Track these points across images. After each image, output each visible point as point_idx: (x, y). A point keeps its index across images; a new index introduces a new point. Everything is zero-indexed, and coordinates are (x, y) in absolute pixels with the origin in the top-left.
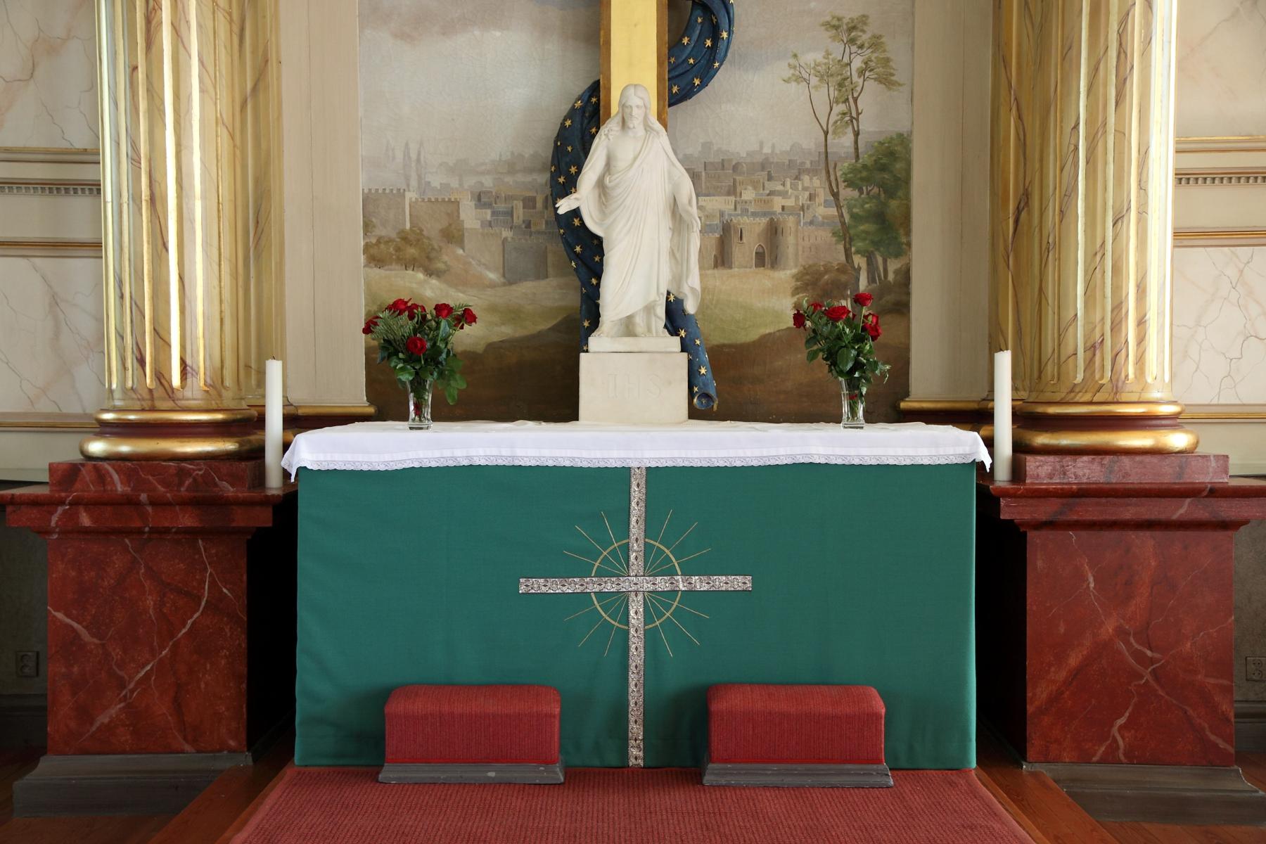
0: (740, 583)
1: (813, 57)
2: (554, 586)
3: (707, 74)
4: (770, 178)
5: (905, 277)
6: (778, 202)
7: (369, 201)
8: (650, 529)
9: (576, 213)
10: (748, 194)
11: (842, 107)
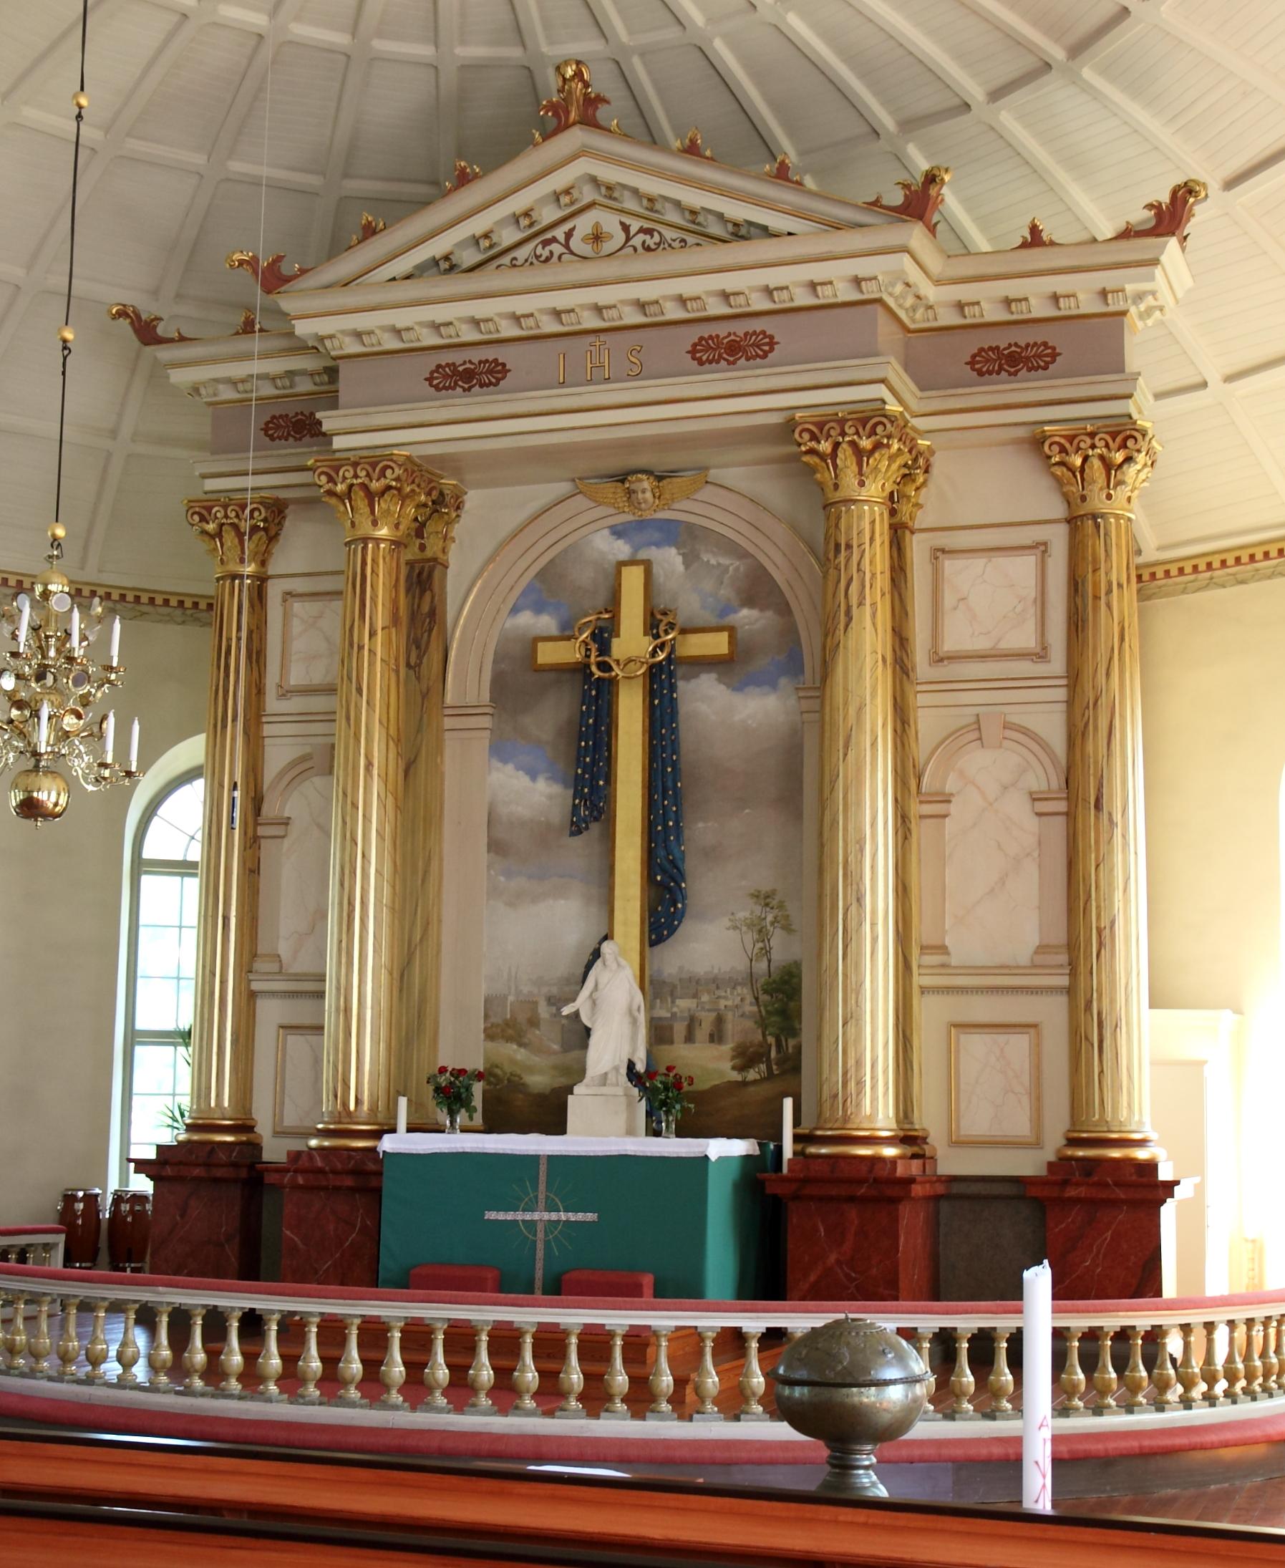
0: (591, 1217)
1: (742, 915)
2: (501, 1216)
3: (672, 930)
4: (718, 988)
5: (798, 1049)
6: (723, 1003)
7: (488, 1001)
8: (548, 1188)
9: (576, 1015)
10: (705, 998)
11: (761, 945)
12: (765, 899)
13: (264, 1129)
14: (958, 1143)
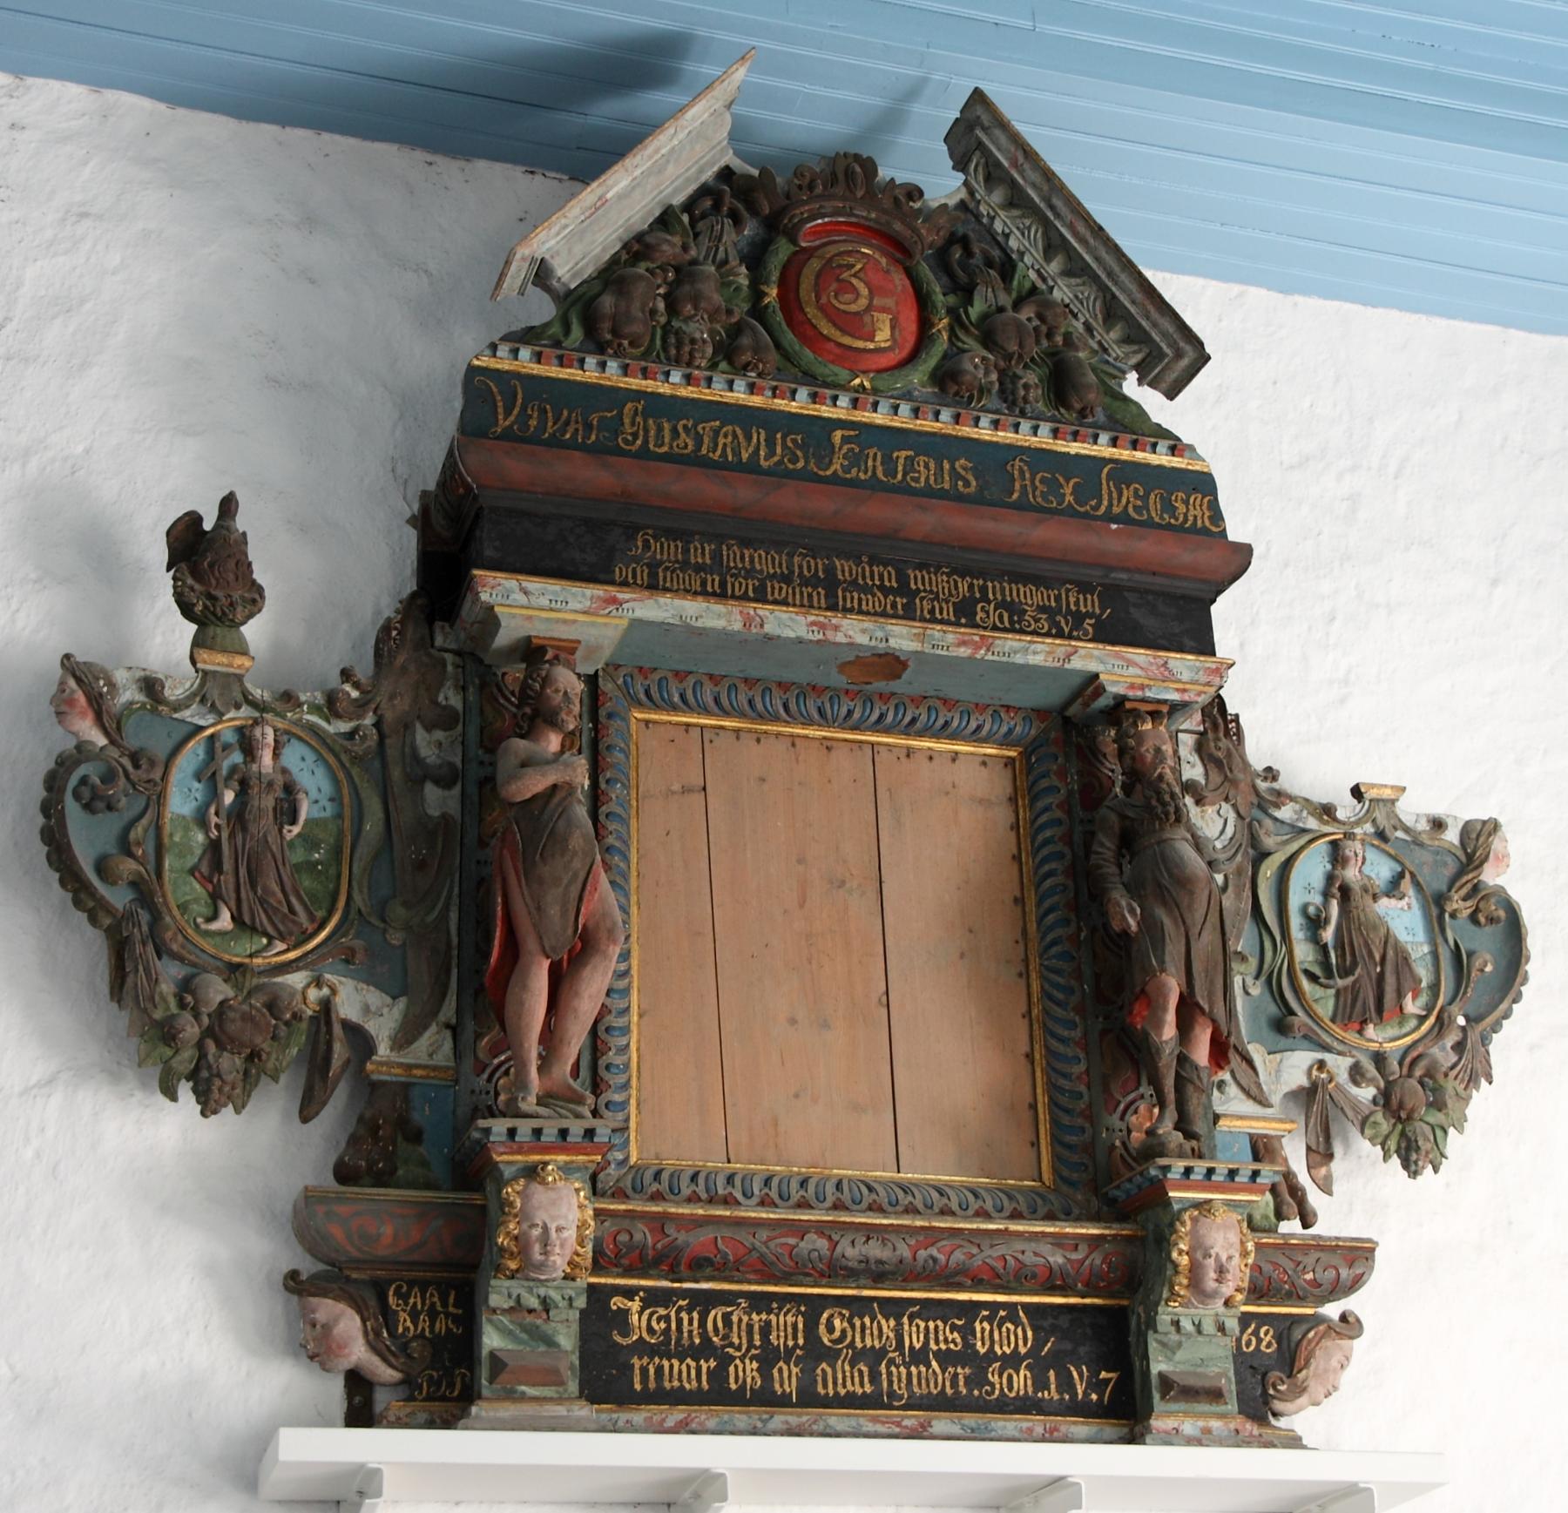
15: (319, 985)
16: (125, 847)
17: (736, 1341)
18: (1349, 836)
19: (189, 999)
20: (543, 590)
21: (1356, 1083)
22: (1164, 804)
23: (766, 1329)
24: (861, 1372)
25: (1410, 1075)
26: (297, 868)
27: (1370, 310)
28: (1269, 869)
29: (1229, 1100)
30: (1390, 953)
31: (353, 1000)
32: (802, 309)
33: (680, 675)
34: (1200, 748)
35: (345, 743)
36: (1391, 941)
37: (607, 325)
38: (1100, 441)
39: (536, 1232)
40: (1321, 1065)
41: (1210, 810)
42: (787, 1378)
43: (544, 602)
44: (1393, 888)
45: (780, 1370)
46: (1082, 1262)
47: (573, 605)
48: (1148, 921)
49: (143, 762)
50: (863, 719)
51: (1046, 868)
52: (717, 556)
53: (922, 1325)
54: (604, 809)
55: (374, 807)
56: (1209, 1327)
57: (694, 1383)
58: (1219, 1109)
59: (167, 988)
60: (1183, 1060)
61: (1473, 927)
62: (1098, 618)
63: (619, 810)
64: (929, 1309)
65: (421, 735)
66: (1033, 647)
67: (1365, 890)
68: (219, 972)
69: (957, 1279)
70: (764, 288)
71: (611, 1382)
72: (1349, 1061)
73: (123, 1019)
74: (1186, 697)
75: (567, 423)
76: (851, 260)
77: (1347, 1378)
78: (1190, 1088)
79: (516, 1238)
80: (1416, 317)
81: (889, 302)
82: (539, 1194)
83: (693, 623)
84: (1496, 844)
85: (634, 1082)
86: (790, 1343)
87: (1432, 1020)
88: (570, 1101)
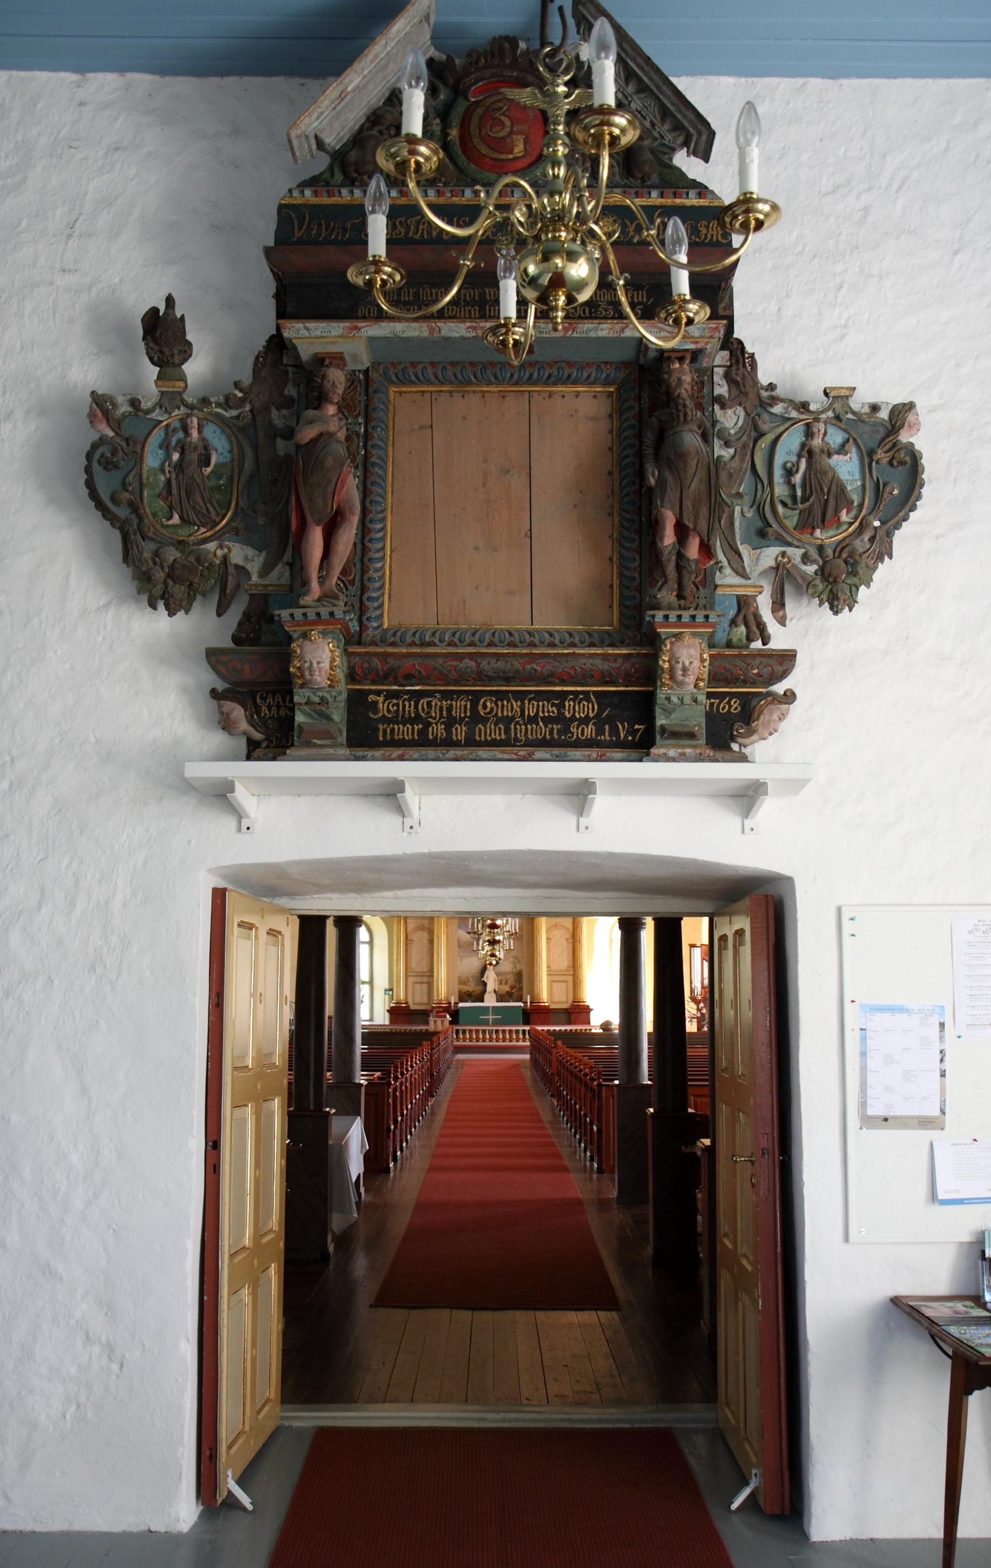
12: (515, 957)
13: (410, 1003)
14: (414, 1004)
15: (222, 548)
16: (124, 486)
17: (433, 715)
18: (817, 420)
19: (157, 560)
20: (318, 328)
21: (805, 563)
22: (678, 411)
23: (450, 709)
24: (500, 729)
25: (839, 557)
26: (212, 489)
27: (893, 81)
28: (764, 444)
29: (725, 576)
30: (834, 487)
31: (239, 554)
32: (471, 141)
33: (413, 365)
34: (727, 376)
35: (235, 421)
36: (835, 480)
37: (352, 168)
38: (690, 195)
39: (307, 665)
40: (783, 554)
41: (730, 412)
42: (460, 732)
43: (318, 333)
44: (842, 450)
45: (456, 729)
46: (619, 668)
47: (334, 333)
48: (661, 482)
49: (131, 443)
50: (520, 378)
51: (625, 453)
52: (416, 295)
53: (536, 704)
54: (370, 443)
55: (249, 453)
56: (688, 700)
57: (410, 737)
58: (718, 582)
59: (147, 555)
60: (680, 556)
61: (890, 469)
62: (645, 304)
63: (380, 443)
64: (539, 696)
65: (274, 413)
66: (601, 326)
67: (822, 451)
68: (173, 545)
69: (550, 679)
70: (449, 131)
71: (364, 737)
72: (802, 551)
73: (128, 571)
74: (699, 346)
75: (333, 229)
76: (501, 105)
77: (783, 726)
78: (685, 572)
79: (299, 668)
80: (924, 81)
81: (524, 127)
82: (308, 646)
83: (401, 335)
84: (911, 418)
85: (387, 586)
86: (463, 715)
87: (857, 524)
88: (333, 598)
